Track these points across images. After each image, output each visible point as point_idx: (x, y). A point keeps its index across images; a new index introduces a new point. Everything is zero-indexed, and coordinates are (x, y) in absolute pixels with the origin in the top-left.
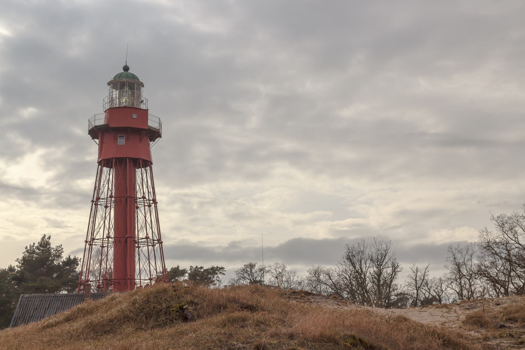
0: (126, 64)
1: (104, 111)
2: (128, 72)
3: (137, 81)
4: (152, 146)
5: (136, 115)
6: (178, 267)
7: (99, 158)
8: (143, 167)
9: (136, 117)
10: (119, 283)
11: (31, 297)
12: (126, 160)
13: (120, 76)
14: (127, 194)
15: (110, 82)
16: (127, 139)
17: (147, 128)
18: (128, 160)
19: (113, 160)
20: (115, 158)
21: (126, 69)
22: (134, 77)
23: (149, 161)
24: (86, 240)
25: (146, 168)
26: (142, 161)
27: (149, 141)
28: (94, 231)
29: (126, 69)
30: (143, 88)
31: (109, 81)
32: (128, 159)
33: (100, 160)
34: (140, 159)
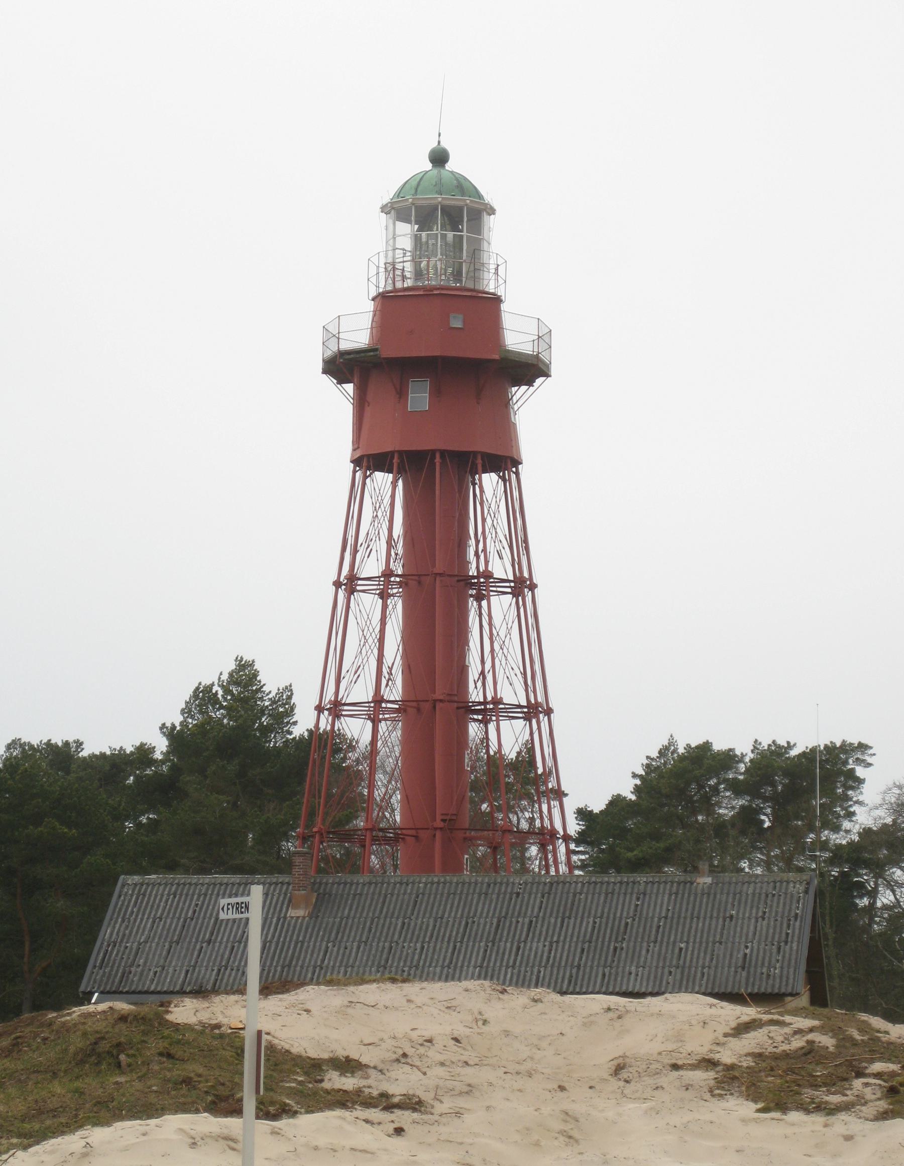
0: (439, 142)
1: (370, 298)
2: (447, 168)
3: (468, 201)
4: (519, 404)
5: (461, 317)
6: (566, 795)
7: (354, 450)
8: (399, 473)
9: (459, 324)
10: (416, 837)
11: (148, 884)
12: (433, 457)
13: (417, 184)
14: (434, 566)
15: (387, 204)
16: (436, 392)
17: (496, 357)
18: (438, 460)
19: (393, 458)
20: (401, 453)
21: (439, 158)
22: (462, 186)
23: (509, 457)
24: (317, 703)
25: (504, 474)
26: (482, 459)
27: (77, 1011)
28: (505, 491)
29: (439, 158)
30: (492, 216)
31: (385, 203)
32: (438, 455)
33: (358, 454)
34: (475, 453)
